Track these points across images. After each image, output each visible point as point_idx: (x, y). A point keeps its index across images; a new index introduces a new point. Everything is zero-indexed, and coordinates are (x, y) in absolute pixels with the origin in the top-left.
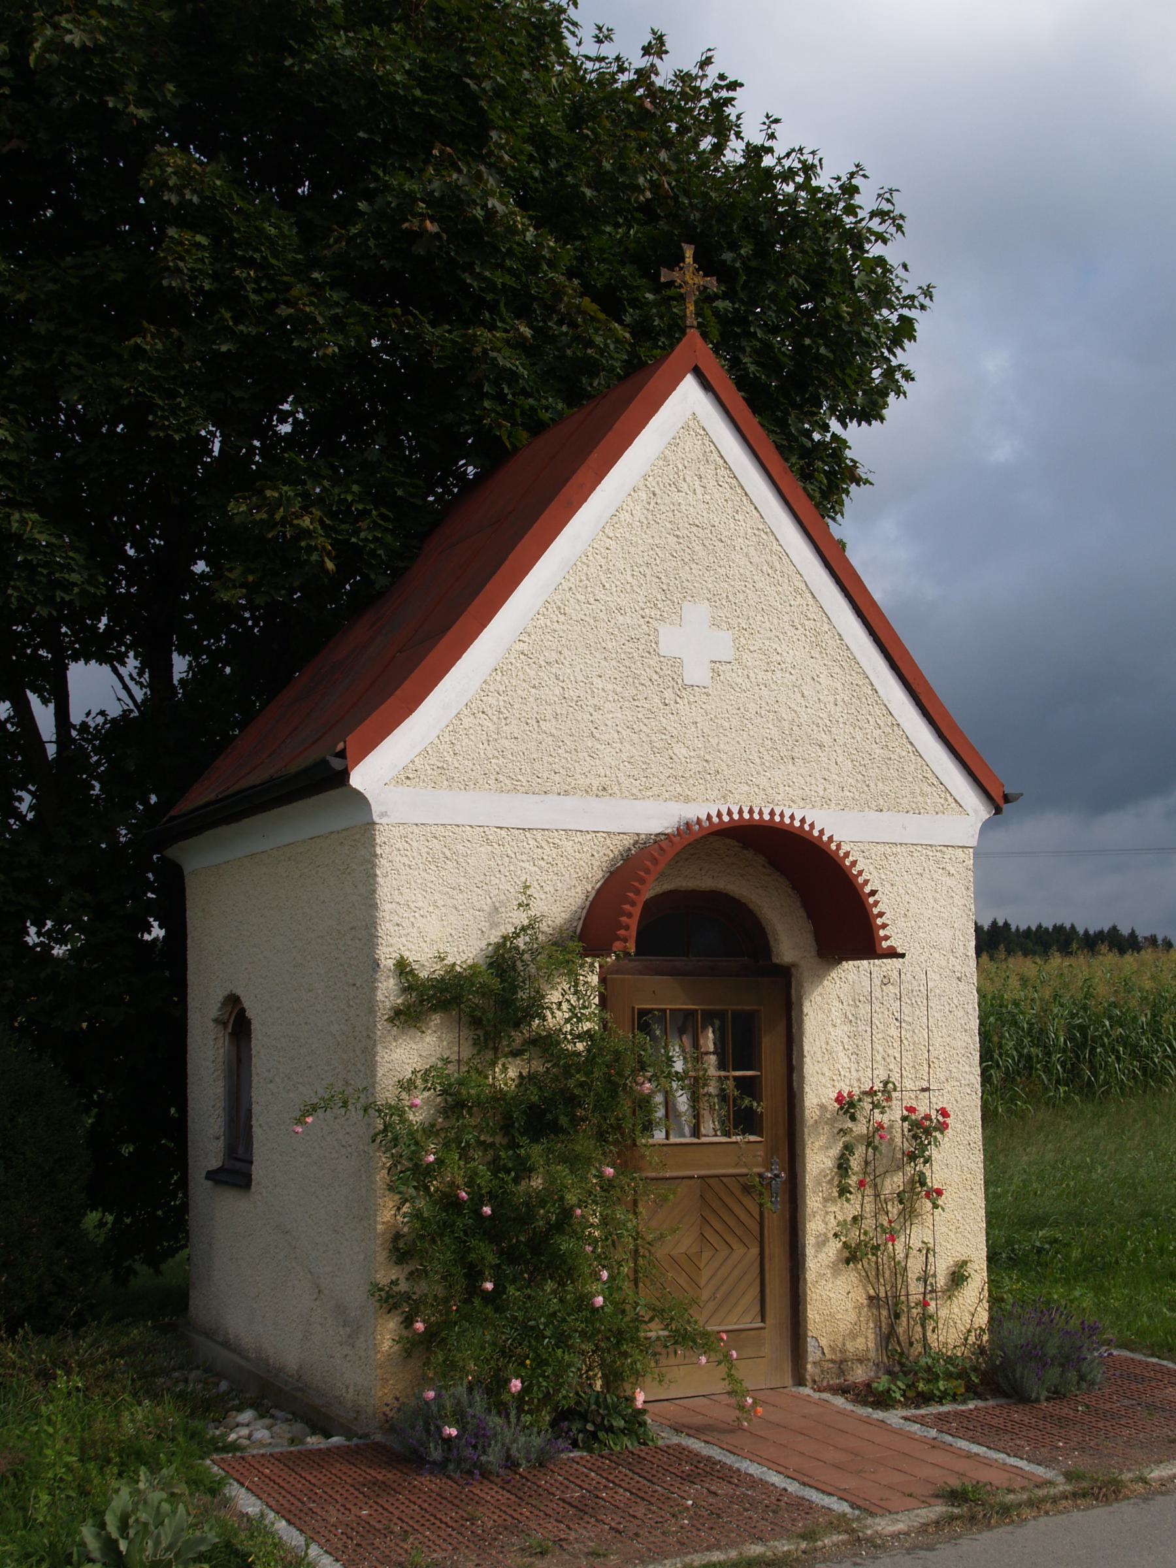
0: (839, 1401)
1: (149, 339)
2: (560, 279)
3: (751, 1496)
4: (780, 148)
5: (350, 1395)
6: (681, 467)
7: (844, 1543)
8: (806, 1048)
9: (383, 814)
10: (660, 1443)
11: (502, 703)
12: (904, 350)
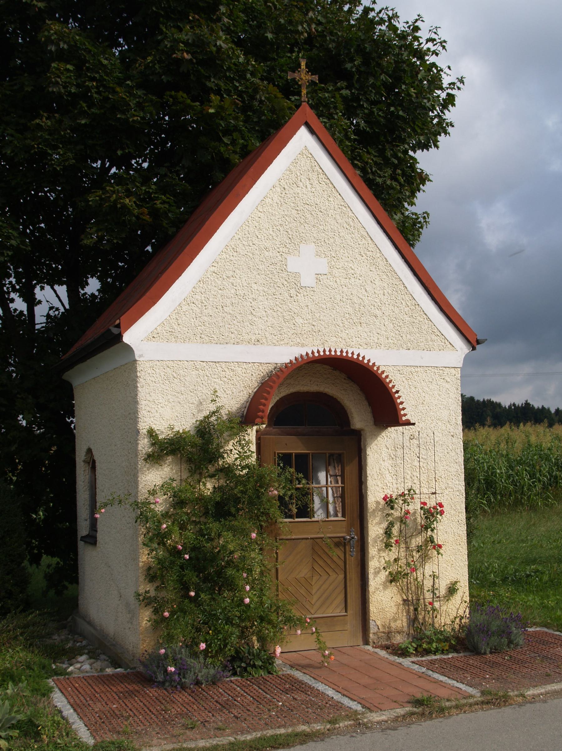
0: (383, 653)
1: (44, 119)
2: (256, 80)
3: (314, 701)
4: (377, 8)
5: (131, 648)
6: (299, 174)
7: (351, 725)
8: (368, 472)
9: (141, 356)
10: (280, 673)
11: (203, 298)
12: (449, 111)
